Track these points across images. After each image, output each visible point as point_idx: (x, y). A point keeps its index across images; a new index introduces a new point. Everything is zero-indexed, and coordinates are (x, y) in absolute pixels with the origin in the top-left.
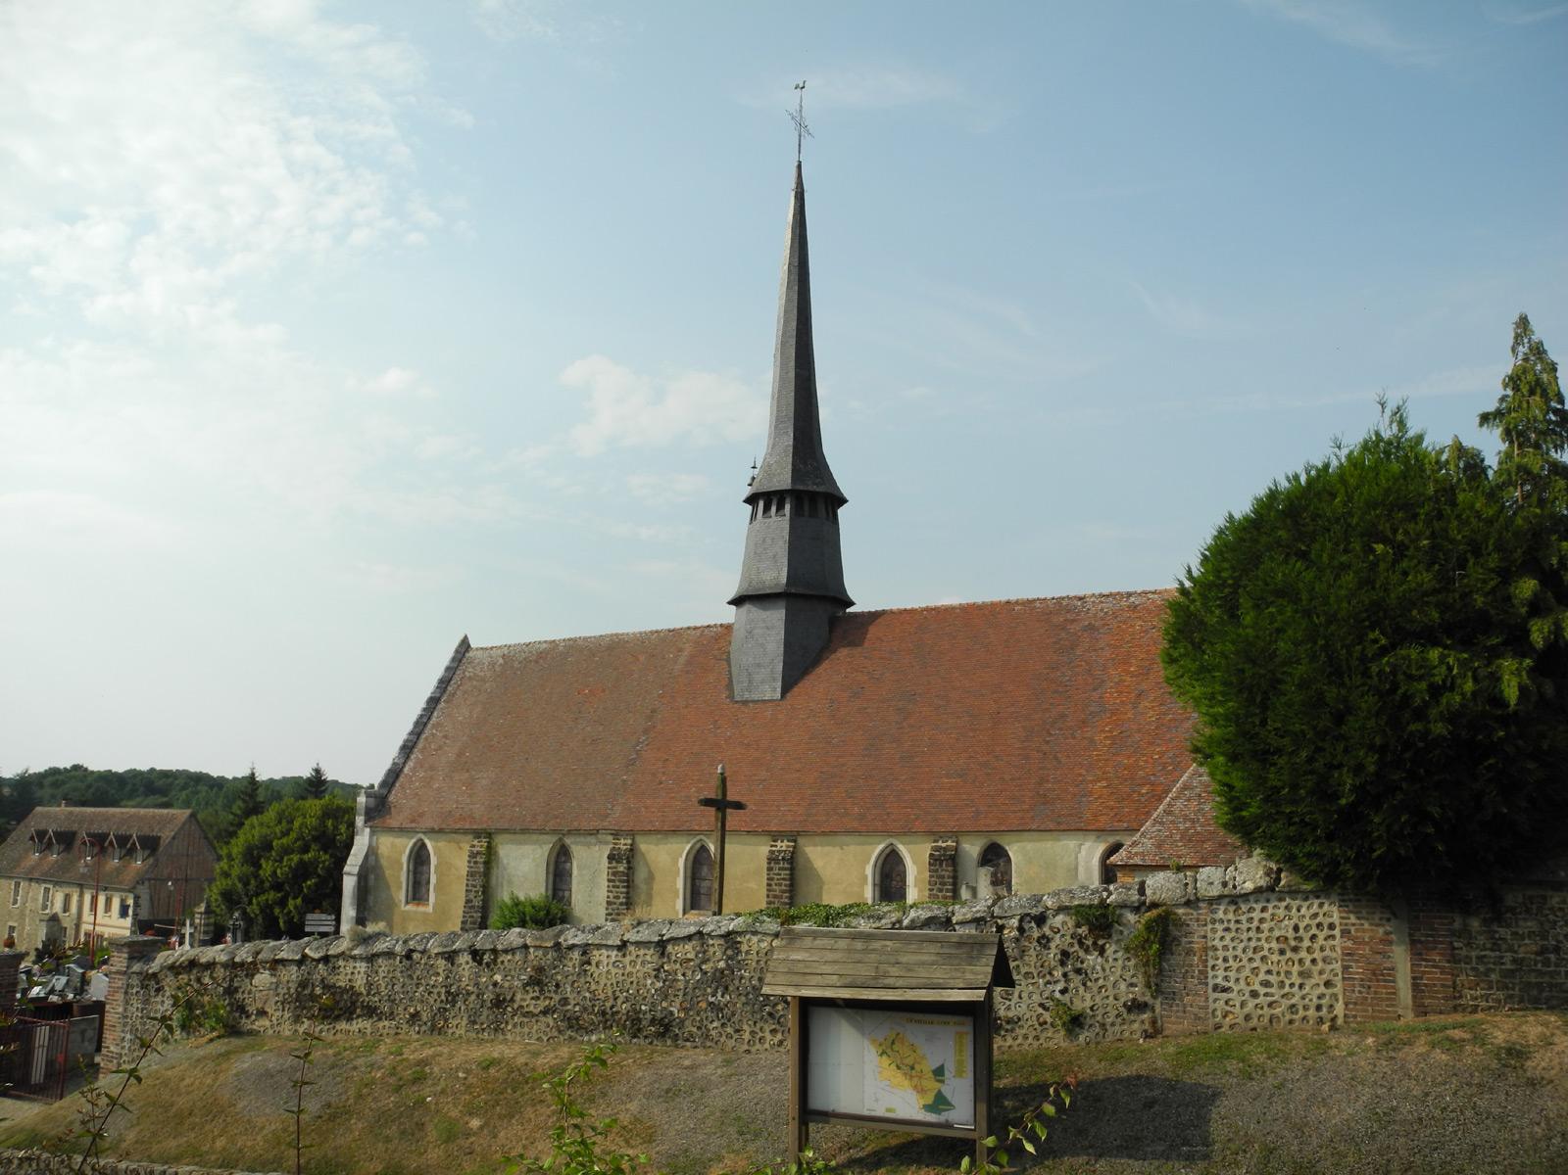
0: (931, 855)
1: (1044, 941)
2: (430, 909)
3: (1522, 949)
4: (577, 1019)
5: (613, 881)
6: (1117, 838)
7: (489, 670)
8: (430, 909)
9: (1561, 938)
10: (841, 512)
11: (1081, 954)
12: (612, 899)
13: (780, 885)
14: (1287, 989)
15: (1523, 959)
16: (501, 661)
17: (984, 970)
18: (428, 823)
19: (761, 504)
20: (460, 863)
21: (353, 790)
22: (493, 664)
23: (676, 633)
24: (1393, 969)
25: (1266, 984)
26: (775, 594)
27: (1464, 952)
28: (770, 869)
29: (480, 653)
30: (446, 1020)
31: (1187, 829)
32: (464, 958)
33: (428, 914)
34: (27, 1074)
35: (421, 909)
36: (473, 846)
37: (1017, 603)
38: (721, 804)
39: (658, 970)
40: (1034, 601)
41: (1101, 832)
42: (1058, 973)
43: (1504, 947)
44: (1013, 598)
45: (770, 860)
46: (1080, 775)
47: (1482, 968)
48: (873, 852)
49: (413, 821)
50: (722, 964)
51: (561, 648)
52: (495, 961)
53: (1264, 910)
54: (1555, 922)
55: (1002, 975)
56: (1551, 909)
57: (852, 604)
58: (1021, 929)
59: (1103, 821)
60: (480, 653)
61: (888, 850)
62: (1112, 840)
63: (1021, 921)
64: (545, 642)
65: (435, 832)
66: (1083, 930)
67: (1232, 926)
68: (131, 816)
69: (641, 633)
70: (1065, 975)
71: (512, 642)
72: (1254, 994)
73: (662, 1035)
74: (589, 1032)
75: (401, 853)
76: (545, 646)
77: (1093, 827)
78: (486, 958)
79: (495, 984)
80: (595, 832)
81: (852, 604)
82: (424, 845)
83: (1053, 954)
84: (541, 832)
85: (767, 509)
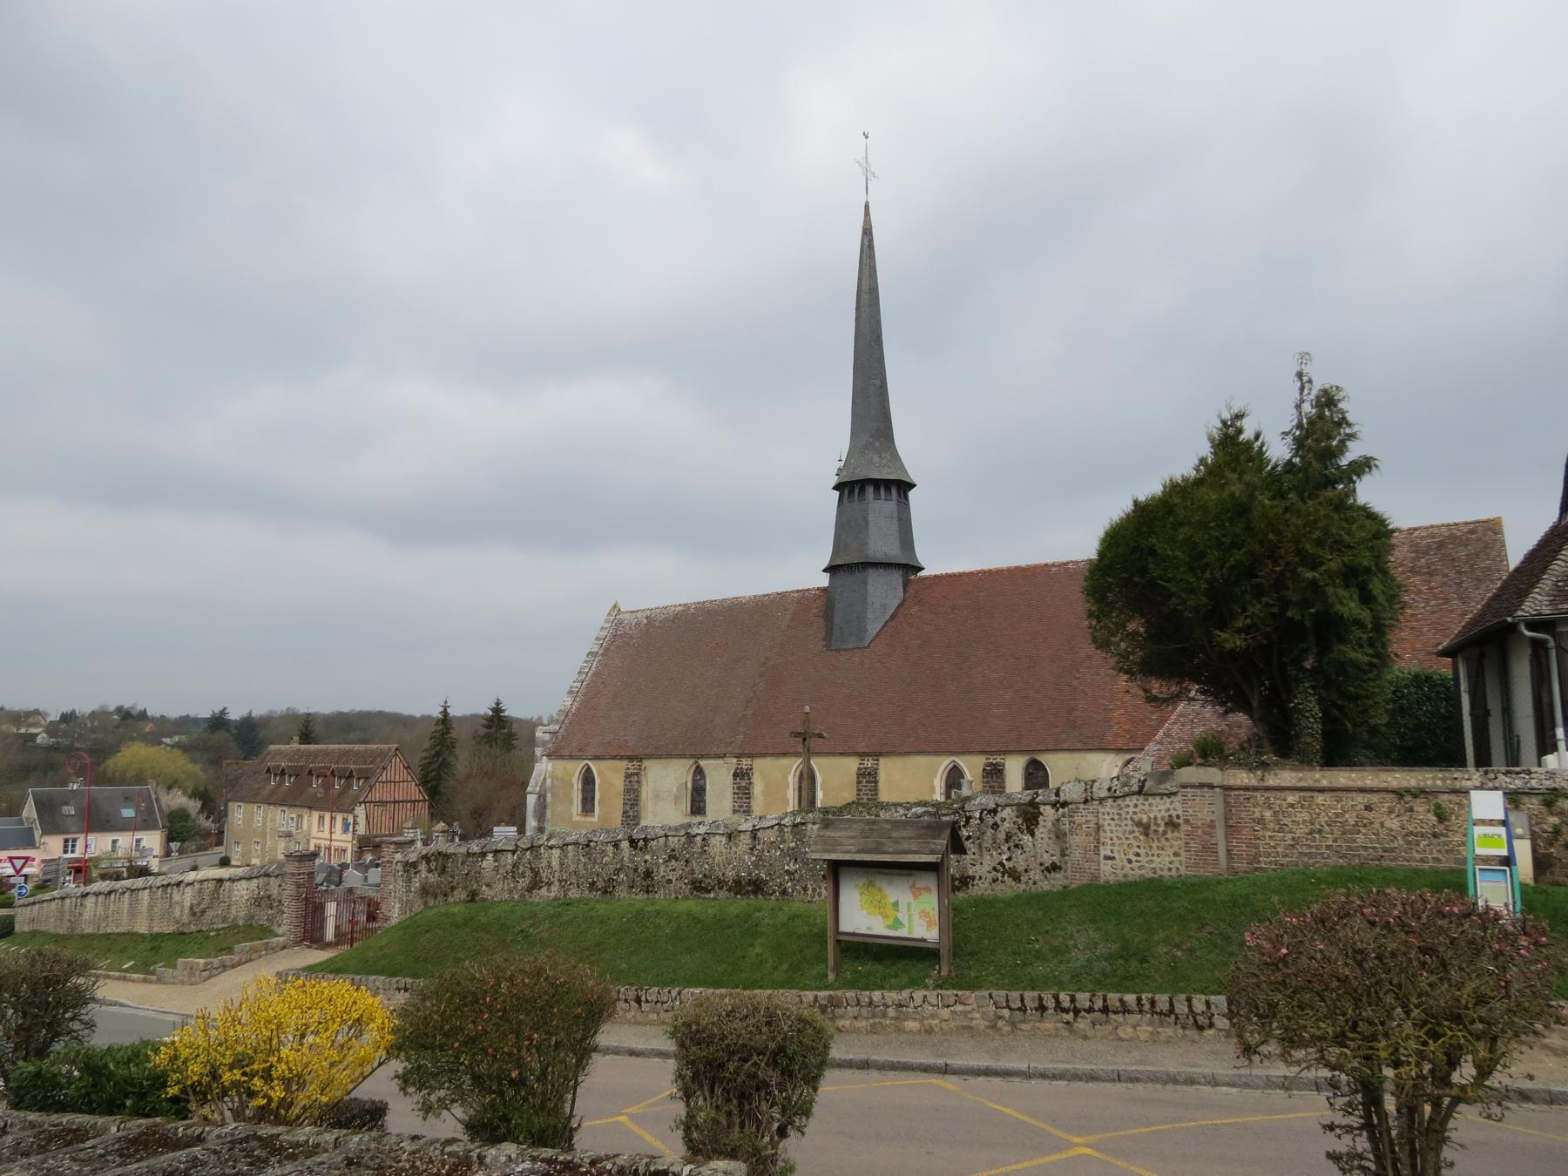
0: (984, 769)
1: (995, 826)
2: (595, 819)
3: (1298, 831)
4: (700, 882)
5: (738, 794)
6: (1133, 756)
7: (636, 628)
8: (595, 819)
9: (1323, 823)
10: (912, 494)
11: (1020, 834)
12: (737, 808)
13: (867, 794)
14: (1150, 858)
15: (1299, 838)
16: (645, 621)
17: (942, 842)
18: (591, 752)
19: (846, 492)
20: (618, 782)
21: (531, 725)
22: (638, 624)
23: (783, 595)
24: (1216, 844)
25: (1138, 855)
26: (857, 564)
27: (1261, 833)
28: (859, 782)
29: (627, 616)
30: (614, 887)
31: (1181, 748)
32: (625, 845)
33: (594, 823)
34: (323, 935)
35: (589, 819)
36: (628, 769)
37: (1053, 565)
38: (804, 737)
39: (752, 849)
40: (1068, 563)
41: (1119, 750)
42: (1005, 848)
43: (1287, 829)
44: (1050, 561)
45: (859, 775)
46: (1104, 705)
47: (1272, 843)
48: (940, 765)
49: (580, 750)
50: (793, 845)
51: (692, 610)
52: (646, 845)
53: (1136, 806)
54: (1319, 814)
55: (957, 846)
56: (1318, 805)
57: (921, 569)
58: (981, 819)
59: (1120, 743)
60: (627, 616)
61: (950, 766)
62: (1128, 757)
63: (981, 813)
64: (680, 605)
65: (596, 758)
66: (1020, 821)
67: (1116, 817)
68: (347, 752)
69: (755, 596)
70: (1009, 849)
71: (653, 606)
72: (1130, 861)
73: (755, 892)
74: (708, 892)
75: (571, 776)
76: (680, 608)
77: (1113, 747)
78: (641, 843)
79: (646, 862)
80: (722, 756)
81: (921, 569)
82: (589, 769)
83: (1001, 836)
84: (683, 756)
85: (851, 492)
